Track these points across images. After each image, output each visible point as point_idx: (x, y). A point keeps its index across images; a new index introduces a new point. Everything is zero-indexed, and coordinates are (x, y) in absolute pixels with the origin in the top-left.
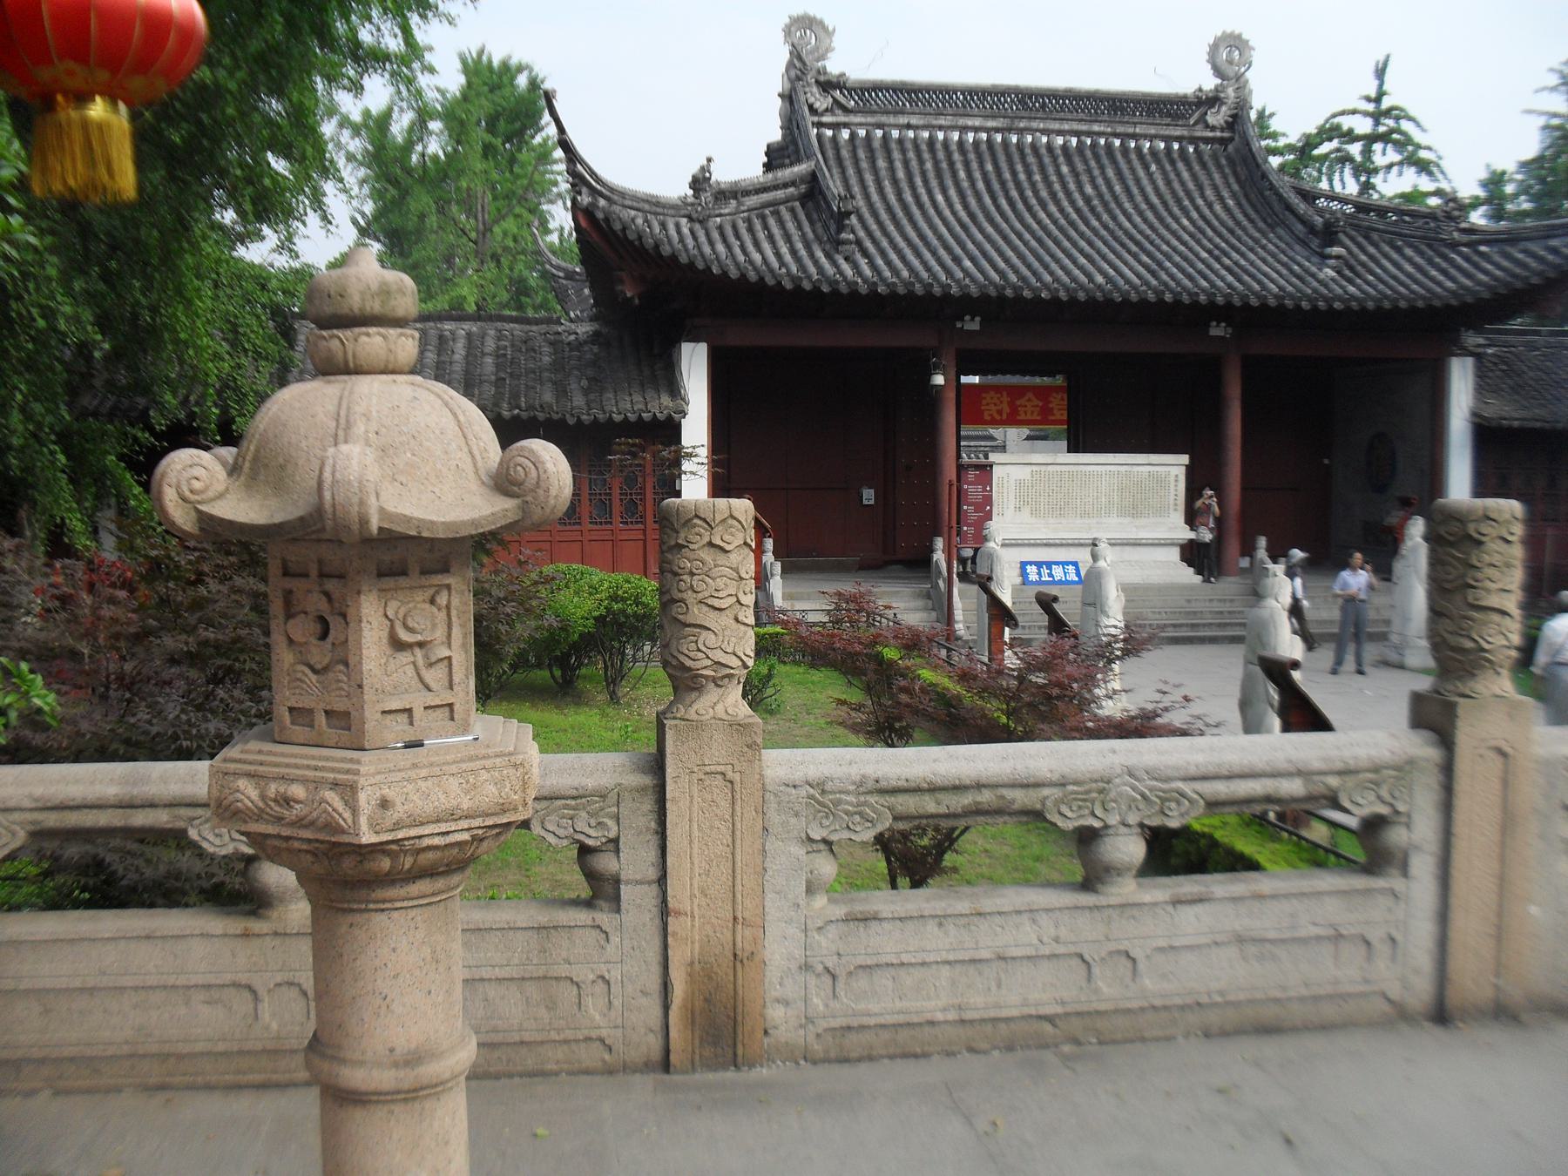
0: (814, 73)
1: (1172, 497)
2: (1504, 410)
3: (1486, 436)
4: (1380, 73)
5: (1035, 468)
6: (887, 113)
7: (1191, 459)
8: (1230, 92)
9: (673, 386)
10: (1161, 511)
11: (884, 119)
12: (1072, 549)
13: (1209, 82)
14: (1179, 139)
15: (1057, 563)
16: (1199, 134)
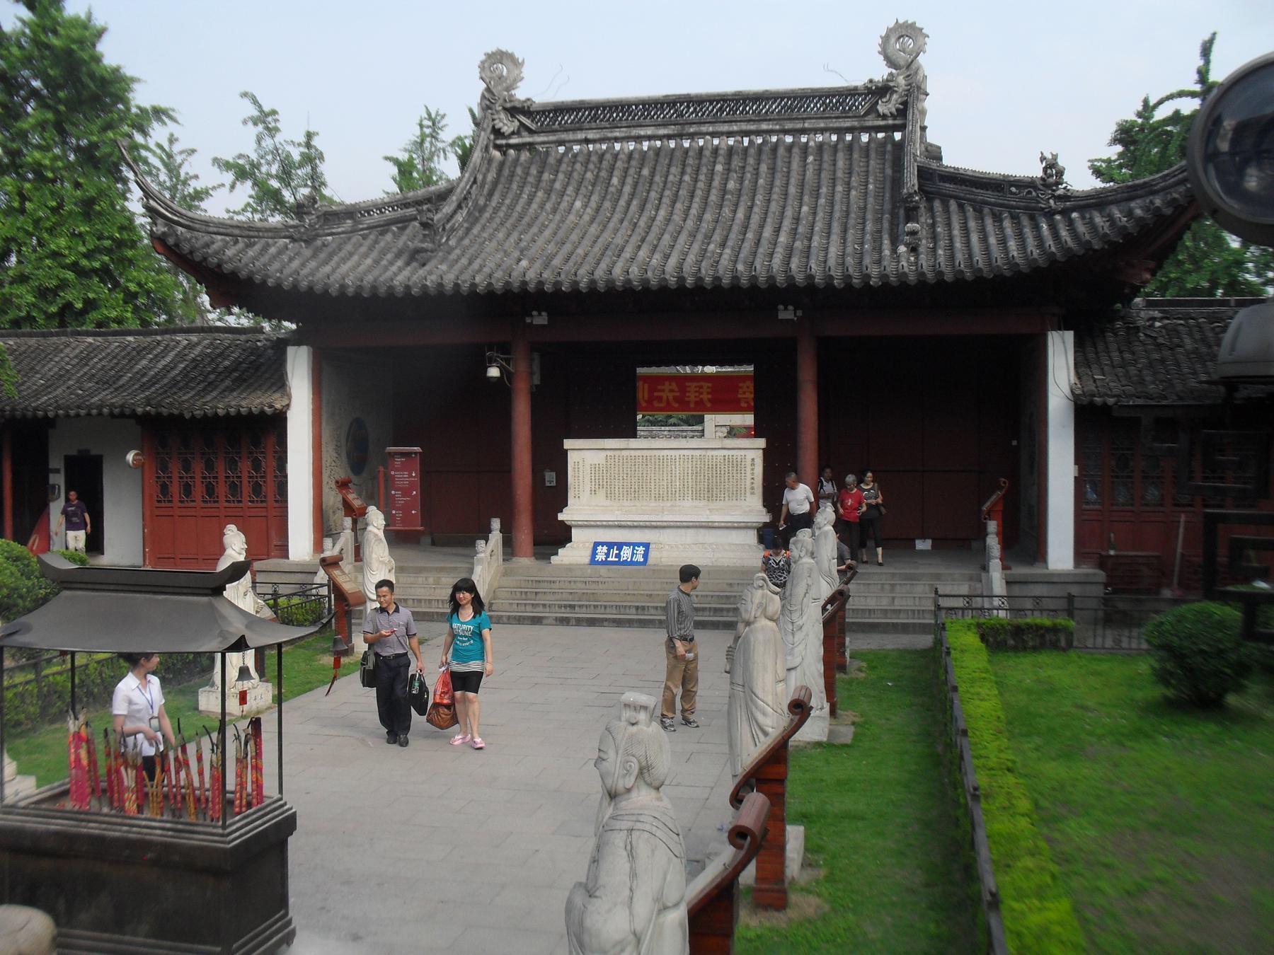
0: (500, 101)
1: (748, 482)
2: (1111, 387)
3: (1088, 415)
4: (1206, 50)
5: (609, 453)
6: (567, 130)
7: (767, 443)
8: (901, 80)
9: (280, 383)
10: (736, 494)
11: (564, 136)
12: (646, 531)
13: (879, 71)
14: (850, 130)
15: (628, 544)
16: (870, 123)
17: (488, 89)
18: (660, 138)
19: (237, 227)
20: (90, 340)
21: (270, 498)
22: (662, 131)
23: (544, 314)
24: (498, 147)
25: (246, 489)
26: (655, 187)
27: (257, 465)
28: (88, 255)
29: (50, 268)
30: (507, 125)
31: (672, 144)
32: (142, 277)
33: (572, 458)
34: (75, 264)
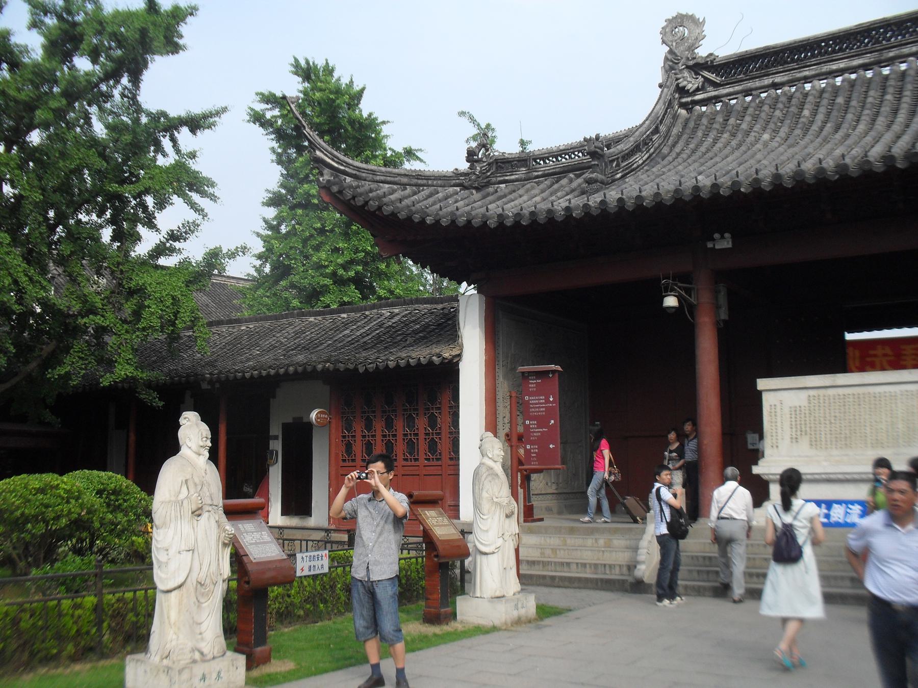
5: (812, 393)
15: (839, 502)
17: (671, 52)
18: (853, 70)
19: (405, 175)
20: (312, 319)
21: (445, 456)
22: (856, 62)
23: (727, 235)
24: (683, 105)
25: (423, 446)
26: (851, 110)
27: (433, 422)
28: (346, 266)
29: (313, 277)
30: (691, 82)
31: (869, 74)
32: (393, 284)
33: (768, 401)
34: (334, 274)
